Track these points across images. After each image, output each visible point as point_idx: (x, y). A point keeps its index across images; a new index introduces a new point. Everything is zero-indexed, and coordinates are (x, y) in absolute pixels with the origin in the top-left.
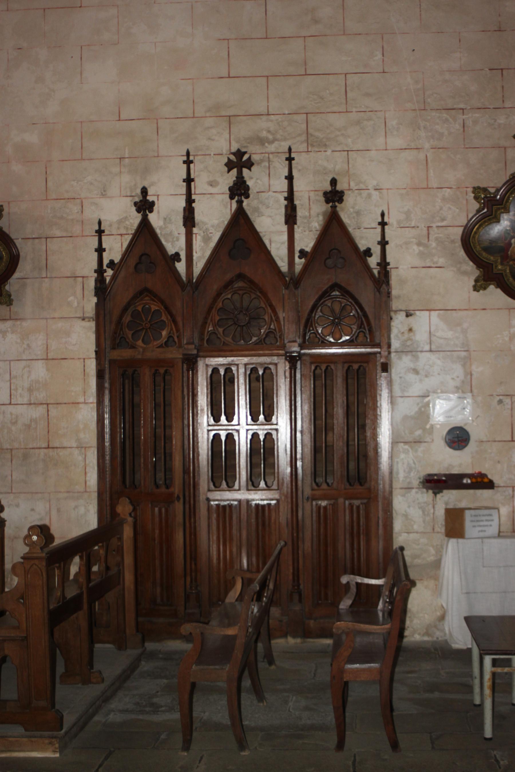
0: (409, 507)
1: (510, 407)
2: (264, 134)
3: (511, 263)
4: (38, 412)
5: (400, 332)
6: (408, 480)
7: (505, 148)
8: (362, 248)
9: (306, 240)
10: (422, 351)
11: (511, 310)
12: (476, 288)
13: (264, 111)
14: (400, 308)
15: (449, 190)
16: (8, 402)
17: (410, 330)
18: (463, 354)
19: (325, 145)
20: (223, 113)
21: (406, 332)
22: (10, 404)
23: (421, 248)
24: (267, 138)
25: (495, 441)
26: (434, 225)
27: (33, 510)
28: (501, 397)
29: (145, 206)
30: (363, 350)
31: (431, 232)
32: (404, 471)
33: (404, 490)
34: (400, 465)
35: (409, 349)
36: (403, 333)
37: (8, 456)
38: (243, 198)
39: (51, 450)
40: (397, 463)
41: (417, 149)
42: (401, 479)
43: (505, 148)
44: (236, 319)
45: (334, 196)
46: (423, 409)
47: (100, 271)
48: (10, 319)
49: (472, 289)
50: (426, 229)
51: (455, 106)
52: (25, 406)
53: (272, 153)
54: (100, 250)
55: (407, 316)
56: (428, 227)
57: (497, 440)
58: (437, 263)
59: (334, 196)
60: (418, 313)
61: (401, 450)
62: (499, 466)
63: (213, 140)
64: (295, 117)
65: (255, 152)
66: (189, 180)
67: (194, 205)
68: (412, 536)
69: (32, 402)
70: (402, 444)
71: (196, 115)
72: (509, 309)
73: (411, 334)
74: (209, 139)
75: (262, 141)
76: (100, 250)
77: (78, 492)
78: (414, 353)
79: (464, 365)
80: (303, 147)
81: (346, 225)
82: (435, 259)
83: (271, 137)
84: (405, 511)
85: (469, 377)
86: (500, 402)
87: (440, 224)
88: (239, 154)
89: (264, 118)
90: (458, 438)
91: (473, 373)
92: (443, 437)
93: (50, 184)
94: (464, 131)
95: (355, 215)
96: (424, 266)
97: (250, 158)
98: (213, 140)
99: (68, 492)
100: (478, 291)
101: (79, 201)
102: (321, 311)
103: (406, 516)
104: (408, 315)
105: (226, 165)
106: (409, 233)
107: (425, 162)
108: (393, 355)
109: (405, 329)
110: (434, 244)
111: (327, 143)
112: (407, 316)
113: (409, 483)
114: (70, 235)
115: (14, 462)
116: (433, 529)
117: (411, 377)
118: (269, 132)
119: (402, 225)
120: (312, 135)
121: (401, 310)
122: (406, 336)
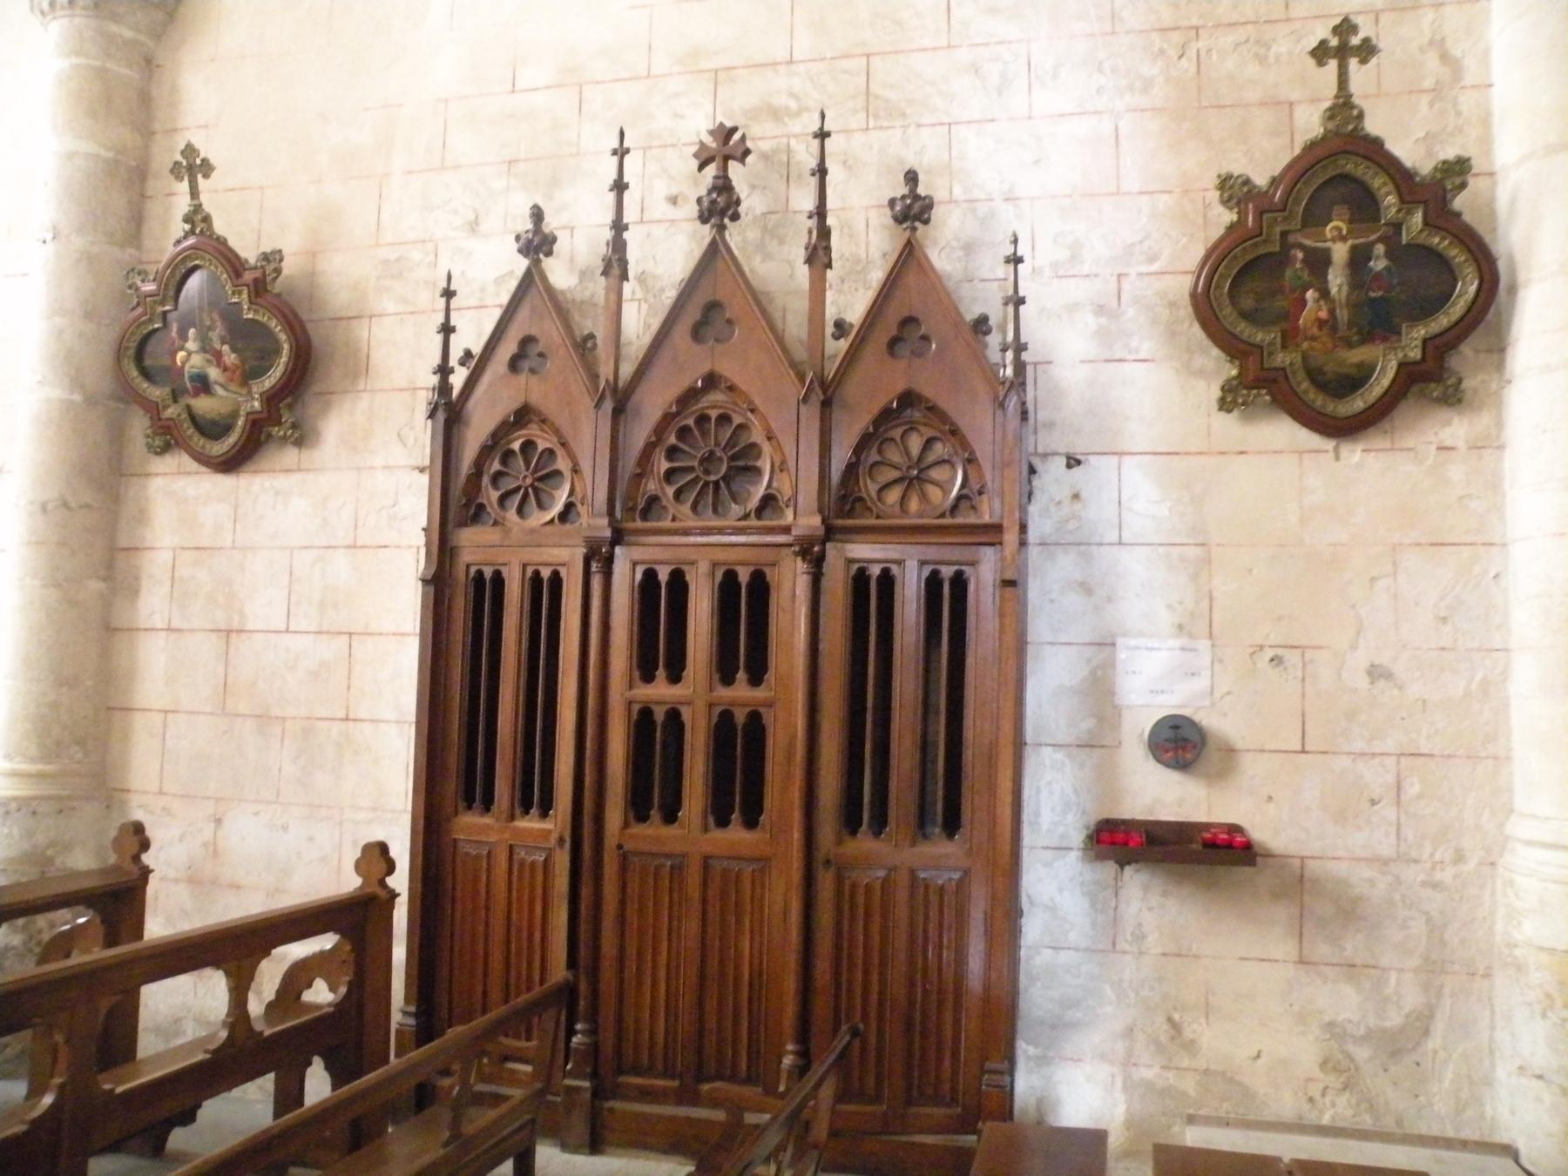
0: (1061, 890)
1: (1300, 674)
2: (781, 100)
3: (1305, 345)
4: (332, 649)
5: (1052, 500)
6: (1061, 829)
7: (1291, 104)
8: (971, 313)
9: (850, 300)
10: (1100, 544)
11: (1306, 456)
12: (1225, 405)
13: (782, 55)
14: (1054, 447)
15: (1165, 197)
16: (283, 627)
17: (1076, 496)
18: (1194, 552)
19: (903, 115)
20: (705, 65)
21: (1066, 502)
22: (287, 631)
23: (1103, 320)
24: (787, 108)
25: (1263, 751)
26: (1133, 271)
27: (311, 839)
28: (1279, 652)
29: (538, 244)
30: (399, 953)
31: (1126, 286)
32: (1053, 810)
33: (1050, 853)
34: (1044, 794)
35: (1071, 539)
36: (1059, 503)
37: (277, 730)
38: (726, 221)
39: (351, 724)
40: (1038, 790)
41: (1096, 112)
42: (1045, 827)
43: (1291, 104)
44: (496, 466)
45: (913, 210)
46: (1099, 673)
47: (444, 370)
48: (299, 470)
49: (1215, 405)
50: (1114, 279)
51: (1180, 23)
52: (312, 636)
53: (795, 136)
54: (447, 330)
55: (1069, 466)
56: (1119, 276)
57: (1267, 747)
58: (1137, 352)
59: (913, 210)
60: (1092, 459)
61: (1047, 761)
62: (1271, 809)
63: (682, 117)
64: (845, 64)
65: (761, 137)
66: (620, 187)
67: (626, 235)
68: (1064, 957)
69: (325, 629)
70: (1050, 749)
71: (654, 72)
72: (1301, 453)
73: (1077, 506)
74: (676, 115)
75: (776, 114)
76: (447, 330)
77: (393, 811)
78: (1083, 548)
79: (1195, 577)
80: (857, 121)
81: (1221, 869)
82: (1134, 343)
83: (793, 105)
84: (1052, 900)
85: (1206, 603)
86: (1276, 660)
87: (1143, 269)
88: (725, 134)
89: (782, 69)
90: (1180, 743)
91: (1215, 594)
92: (1141, 735)
93: (385, 215)
94: (1199, 72)
95: (961, 253)
96: (1108, 356)
97: (743, 138)
98: (682, 117)
99: (374, 809)
100: (1229, 411)
101: (430, 246)
102: (880, 452)
103: (1052, 909)
104: (1073, 462)
105: (696, 155)
106: (1077, 290)
107: (1113, 140)
108: (1033, 553)
109: (1066, 493)
110: (1131, 312)
111: (908, 111)
112: (1069, 466)
113: (1062, 837)
114: (410, 309)
115: (286, 742)
116: (1114, 944)
117: (1073, 600)
118: (792, 95)
119: (1061, 272)
120: (877, 97)
121: (1056, 454)
122: (1066, 509)
